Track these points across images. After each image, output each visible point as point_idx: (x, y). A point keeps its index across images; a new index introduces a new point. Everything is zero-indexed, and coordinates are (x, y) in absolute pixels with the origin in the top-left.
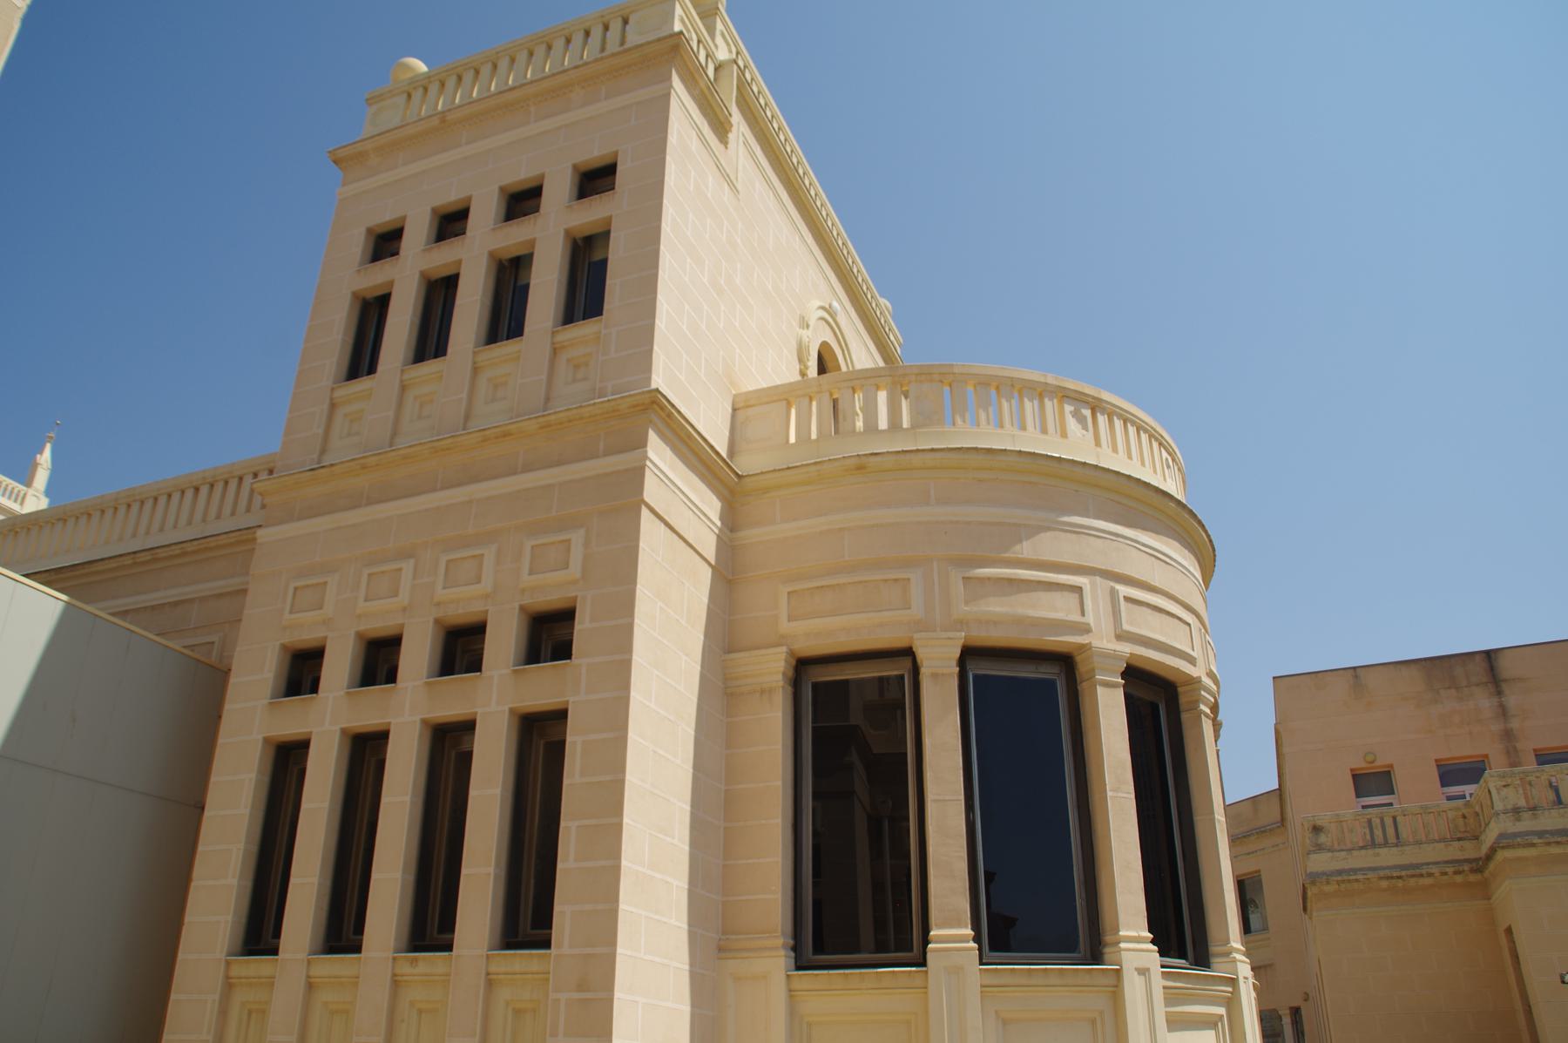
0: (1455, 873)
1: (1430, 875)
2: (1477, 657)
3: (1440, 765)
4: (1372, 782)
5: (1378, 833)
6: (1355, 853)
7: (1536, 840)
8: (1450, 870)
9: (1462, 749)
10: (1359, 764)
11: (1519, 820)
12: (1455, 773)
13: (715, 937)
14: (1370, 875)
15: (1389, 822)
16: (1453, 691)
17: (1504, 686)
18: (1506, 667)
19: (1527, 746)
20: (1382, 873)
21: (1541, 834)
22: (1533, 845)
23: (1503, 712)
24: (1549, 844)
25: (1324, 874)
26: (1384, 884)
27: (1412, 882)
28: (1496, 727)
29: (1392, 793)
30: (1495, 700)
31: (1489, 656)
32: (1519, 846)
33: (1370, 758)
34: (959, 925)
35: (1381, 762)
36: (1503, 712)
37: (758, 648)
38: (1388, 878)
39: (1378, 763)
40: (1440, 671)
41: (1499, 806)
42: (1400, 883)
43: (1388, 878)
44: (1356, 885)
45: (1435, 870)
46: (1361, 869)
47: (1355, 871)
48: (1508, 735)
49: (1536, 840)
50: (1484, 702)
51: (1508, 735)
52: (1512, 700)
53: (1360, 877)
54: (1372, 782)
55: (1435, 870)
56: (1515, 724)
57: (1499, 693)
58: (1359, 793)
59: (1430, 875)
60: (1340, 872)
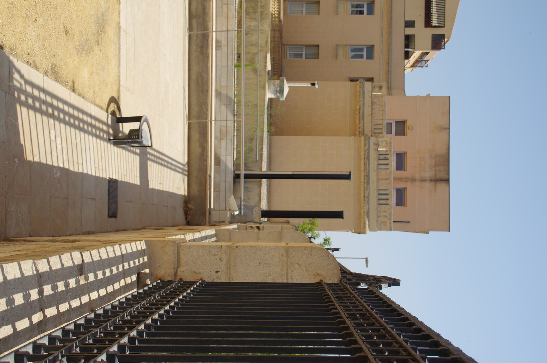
0: (360, 132)
1: (360, 123)
2: (447, 176)
3: (405, 153)
4: (401, 127)
5: (382, 157)
6: (370, 99)
7: (366, 147)
8: (361, 130)
9: (409, 162)
10: (408, 124)
11: (374, 144)
12: (401, 158)
13: (258, 239)
14: (361, 103)
15: (380, 127)
16: (434, 164)
17: (434, 183)
18: (441, 186)
19: (408, 186)
20: (362, 107)
21: (369, 149)
22: (365, 146)
23: (423, 180)
24: (365, 151)
25: (364, 87)
26: (358, 107)
27: (358, 117)
28: (417, 177)
29: (396, 134)
30: (428, 178)
31: (447, 181)
32: (365, 142)
33: (411, 128)
34: (269, 201)
35: (408, 132)
36: (423, 180)
37: (119, 76)
38: (360, 109)
39: (408, 130)
40: (444, 161)
41: (380, 140)
42: (357, 113)
43: (360, 109)
44: (358, 97)
45: (361, 125)
46: (364, 100)
47: (364, 98)
48: (413, 180)
49: (366, 147)
50: (428, 174)
51: (413, 180)
52: (428, 184)
53: (361, 99)
54: (401, 127)
55: (361, 125)
56: (418, 183)
57: (431, 181)
58: (397, 123)
59: (360, 123)
60: (364, 92)
